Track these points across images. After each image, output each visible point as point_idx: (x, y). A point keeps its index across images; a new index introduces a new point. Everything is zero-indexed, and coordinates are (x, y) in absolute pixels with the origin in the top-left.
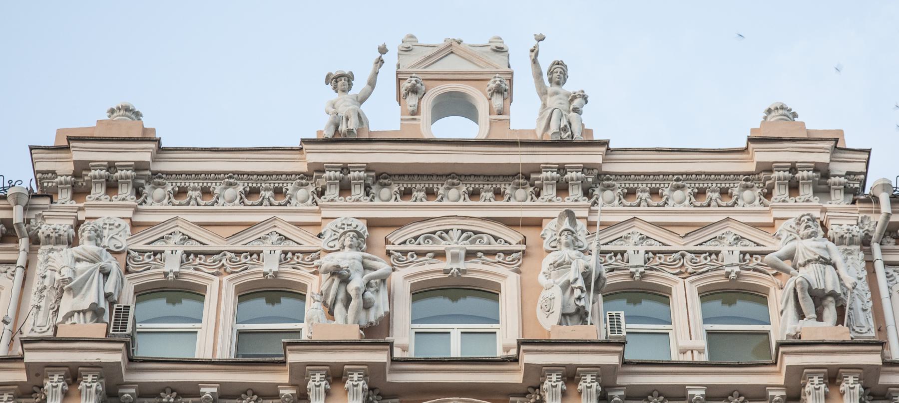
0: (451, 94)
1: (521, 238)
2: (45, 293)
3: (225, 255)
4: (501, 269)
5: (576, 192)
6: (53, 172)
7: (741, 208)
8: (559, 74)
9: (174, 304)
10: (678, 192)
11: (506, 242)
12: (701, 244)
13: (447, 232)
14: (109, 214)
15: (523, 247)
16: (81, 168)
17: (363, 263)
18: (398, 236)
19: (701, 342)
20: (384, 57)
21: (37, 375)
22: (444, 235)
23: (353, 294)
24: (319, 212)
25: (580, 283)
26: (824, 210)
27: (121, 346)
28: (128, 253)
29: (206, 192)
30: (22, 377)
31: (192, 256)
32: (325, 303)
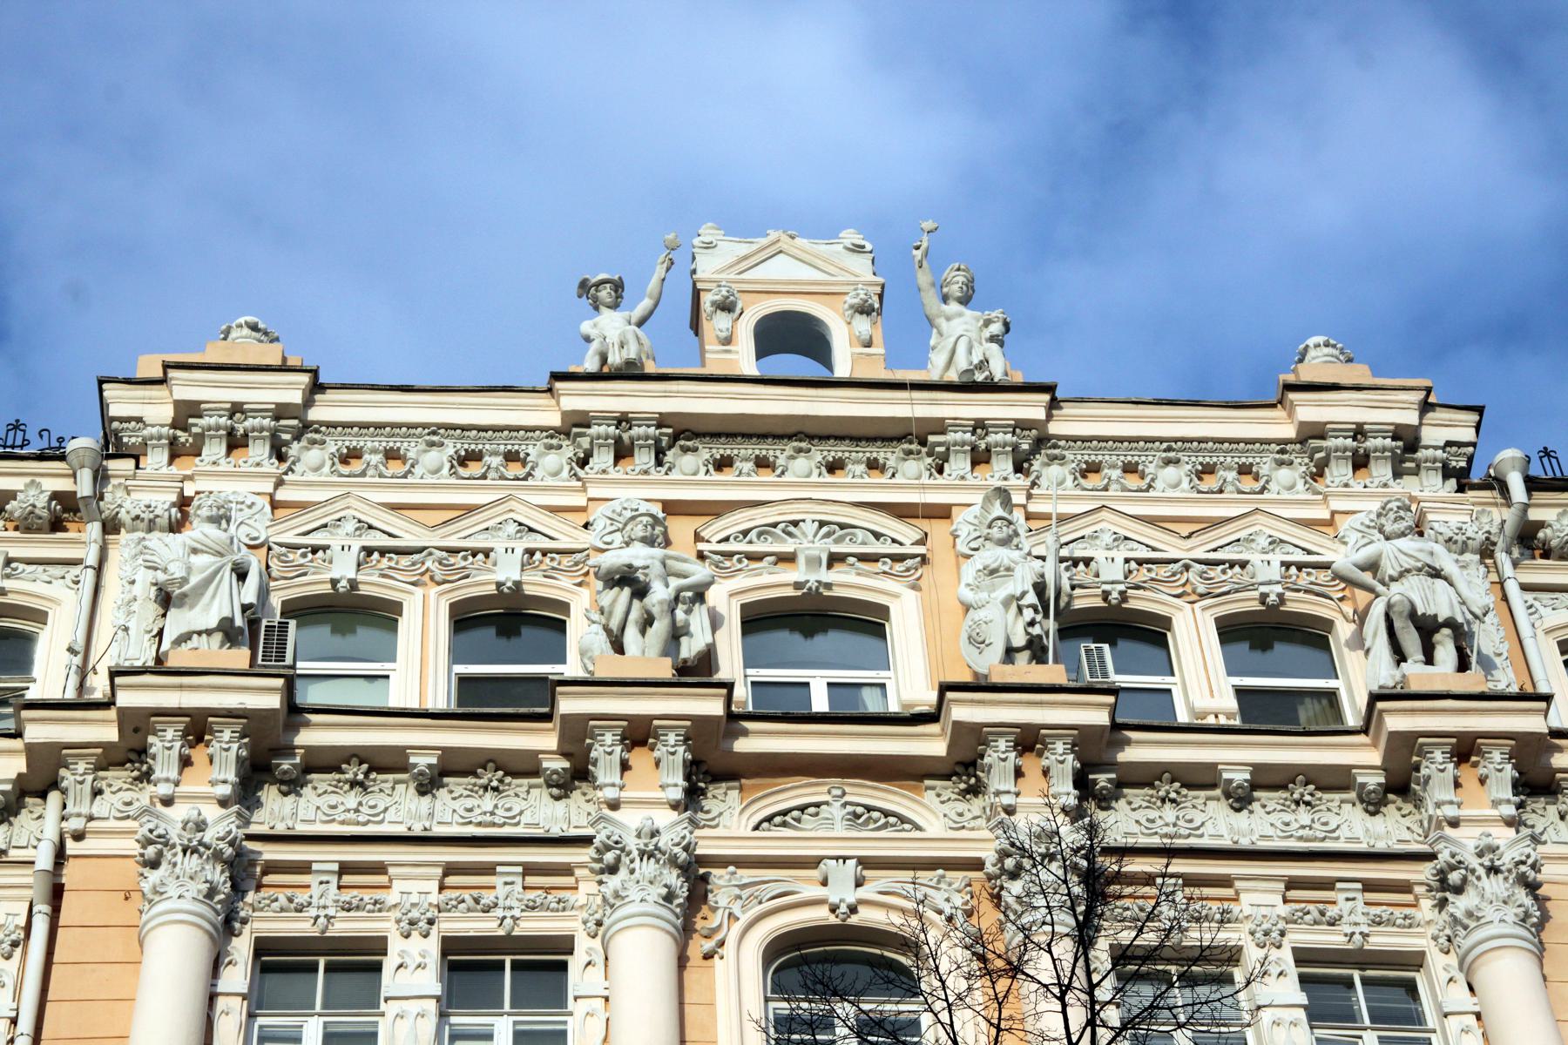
1: (917, 536)
2: (135, 607)
3: (430, 554)
5: (1003, 466)
6: (139, 420)
7: (1275, 496)
9: (344, 634)
10: (1171, 469)
11: (894, 541)
12: (1215, 550)
13: (795, 523)
16: (187, 412)
17: (664, 565)
18: (715, 530)
19: (1232, 704)
21: (136, 730)
22: (791, 529)
23: (655, 611)
24: (584, 489)
25: (1031, 598)
27: (280, 682)
28: (270, 549)
30: (111, 734)
32: (607, 629)
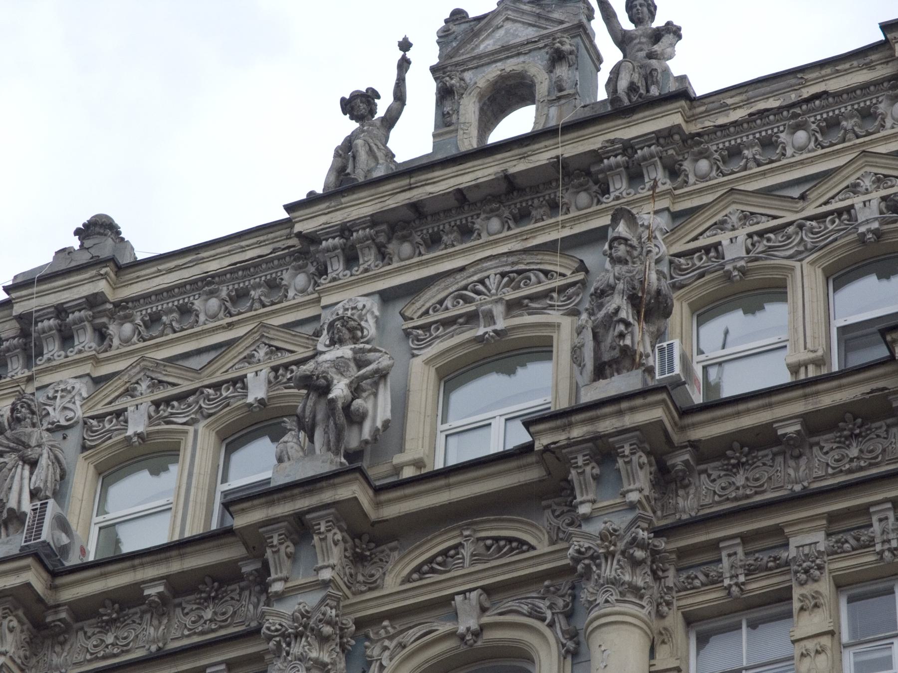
0: (503, 78)
9: (753, 313)
13: (482, 282)
15: (581, 276)
20: (409, 55)
24: (318, 300)
31: (281, 372)
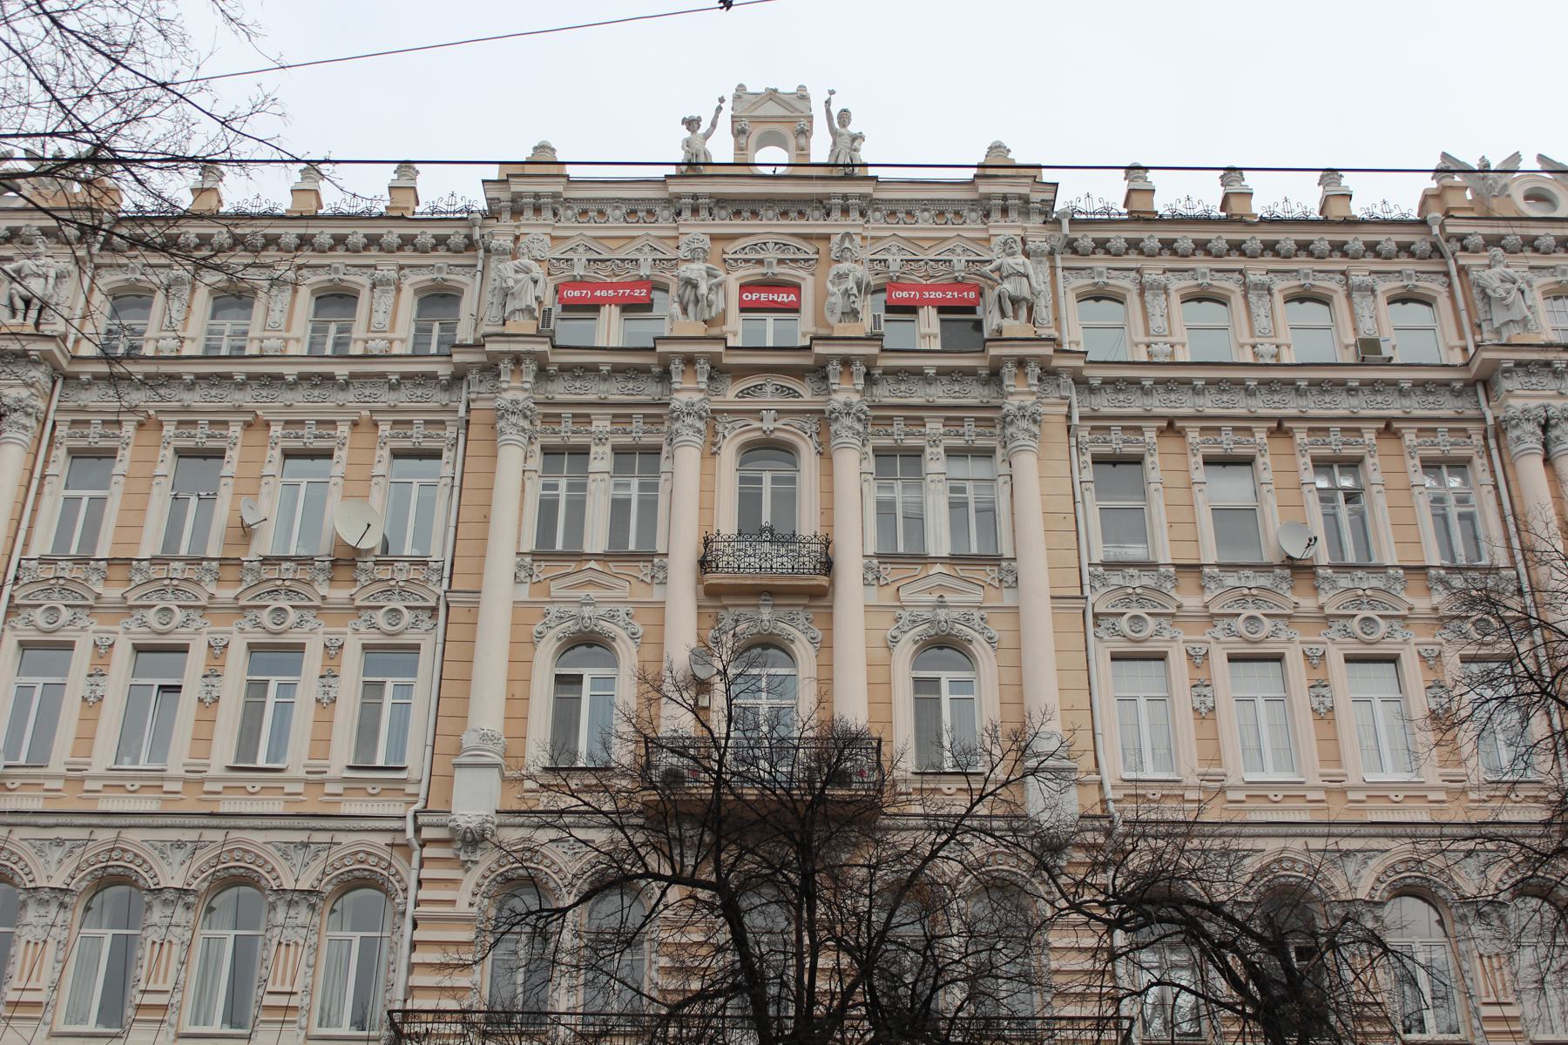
4: (802, 273)
8: (845, 116)
14: (536, 230)
16: (516, 198)
18: (731, 247)
25: (855, 291)
26: (1025, 229)
29: (601, 213)
